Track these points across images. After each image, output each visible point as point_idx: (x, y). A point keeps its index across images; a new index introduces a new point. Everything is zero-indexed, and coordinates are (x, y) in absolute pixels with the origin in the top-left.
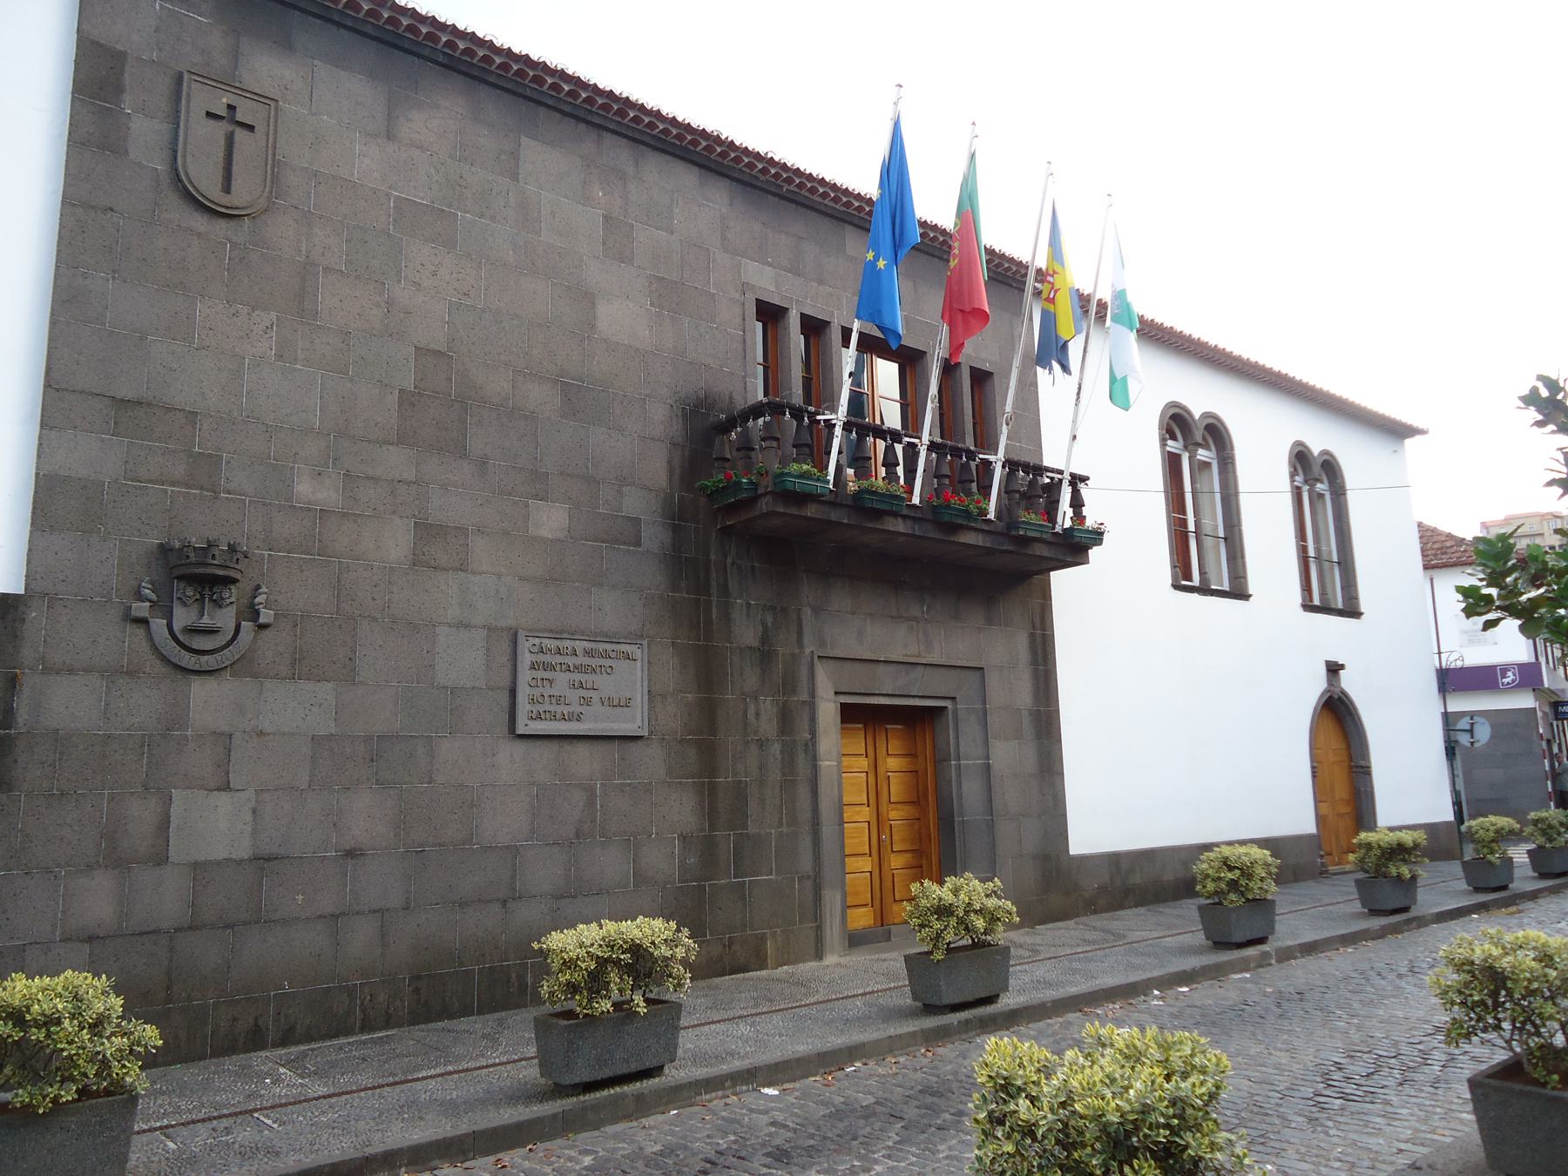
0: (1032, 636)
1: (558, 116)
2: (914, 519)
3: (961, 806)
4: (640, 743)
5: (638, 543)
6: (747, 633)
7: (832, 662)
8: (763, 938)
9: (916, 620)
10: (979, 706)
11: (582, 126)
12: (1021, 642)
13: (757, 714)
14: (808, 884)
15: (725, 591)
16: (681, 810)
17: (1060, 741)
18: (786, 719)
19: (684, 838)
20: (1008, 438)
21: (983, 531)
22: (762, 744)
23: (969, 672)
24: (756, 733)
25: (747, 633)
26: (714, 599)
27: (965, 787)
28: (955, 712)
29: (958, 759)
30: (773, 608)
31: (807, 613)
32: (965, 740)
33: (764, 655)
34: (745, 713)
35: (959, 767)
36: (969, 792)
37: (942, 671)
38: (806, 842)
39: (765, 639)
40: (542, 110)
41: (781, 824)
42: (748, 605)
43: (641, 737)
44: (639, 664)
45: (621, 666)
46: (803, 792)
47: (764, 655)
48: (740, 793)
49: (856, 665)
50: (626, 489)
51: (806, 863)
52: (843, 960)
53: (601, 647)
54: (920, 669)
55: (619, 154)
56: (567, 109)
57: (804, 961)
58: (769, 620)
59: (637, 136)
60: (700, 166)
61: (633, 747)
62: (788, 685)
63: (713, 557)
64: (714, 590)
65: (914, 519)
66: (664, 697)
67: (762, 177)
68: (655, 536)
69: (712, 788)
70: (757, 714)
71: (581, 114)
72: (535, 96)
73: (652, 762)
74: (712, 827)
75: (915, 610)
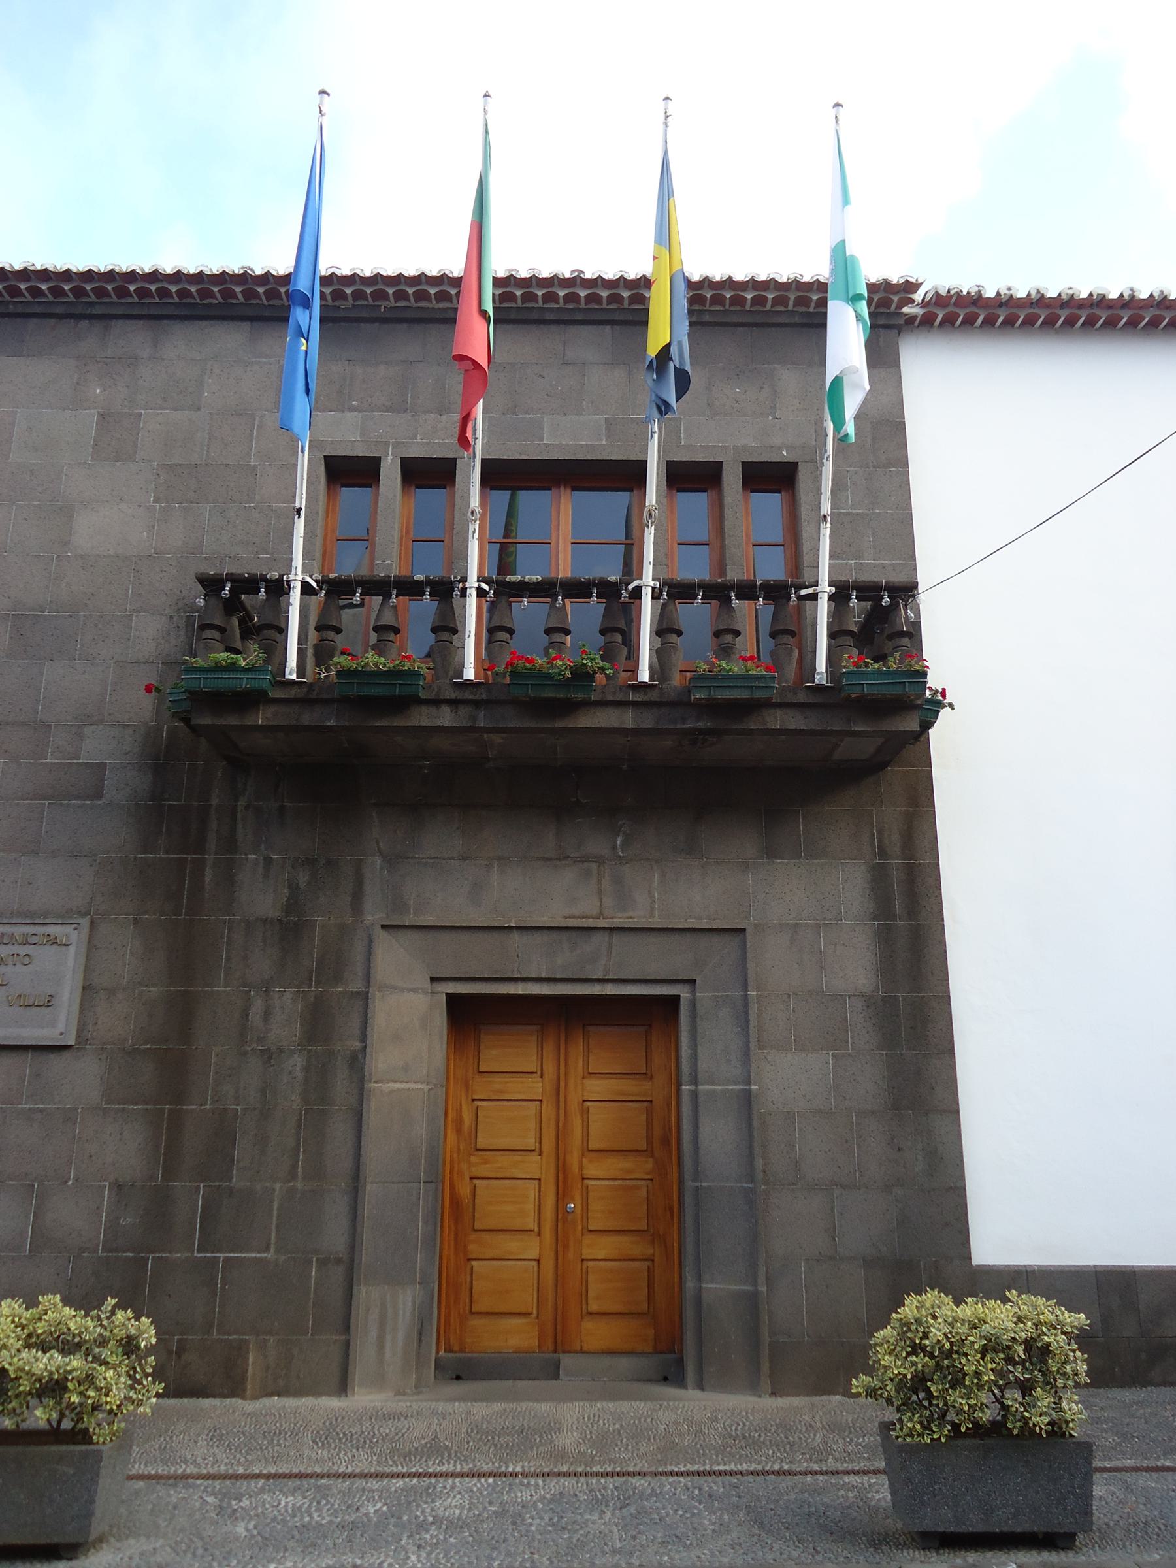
0: (879, 876)
1: (52, 321)
2: (477, 704)
3: (697, 1162)
4: (67, 1055)
5: (98, 795)
6: (261, 898)
7: (415, 935)
8: (241, 1349)
9: (600, 860)
10: (737, 994)
11: (84, 324)
12: (846, 885)
13: (267, 1015)
14: (337, 1274)
15: (230, 844)
16: (121, 1148)
17: (949, 1051)
18: (318, 1023)
19: (118, 1187)
20: (831, 557)
21: (635, 704)
22: (269, 1056)
23: (716, 939)
24: (260, 1040)
25: (261, 898)
26: (210, 858)
27: (705, 1129)
28: (693, 1004)
29: (695, 1081)
30: (311, 862)
31: (374, 865)
32: (709, 1047)
33: (290, 929)
34: (245, 1014)
35: (695, 1095)
36: (715, 1138)
37: (652, 939)
38: (336, 1209)
39: (293, 905)
40: (32, 323)
41: (293, 1176)
42: (268, 861)
43: (70, 1046)
44: (72, 949)
45: (45, 956)
46: (339, 1130)
47: (290, 929)
48: (223, 1129)
49: (465, 937)
50: (88, 730)
51: (334, 1238)
52: (401, 1405)
53: (18, 930)
54: (600, 939)
55: (132, 339)
56: (59, 310)
57: (317, 1393)
58: (303, 879)
59: (153, 311)
60: (252, 319)
61: (56, 1062)
62: (332, 966)
63: (214, 802)
64: (212, 843)
65: (477, 704)
66: (111, 992)
67: (341, 304)
68: (125, 783)
69: (176, 1120)
70: (267, 1015)
71: (79, 310)
72: (20, 309)
73: (82, 1080)
74: (170, 1173)
75: (597, 844)
